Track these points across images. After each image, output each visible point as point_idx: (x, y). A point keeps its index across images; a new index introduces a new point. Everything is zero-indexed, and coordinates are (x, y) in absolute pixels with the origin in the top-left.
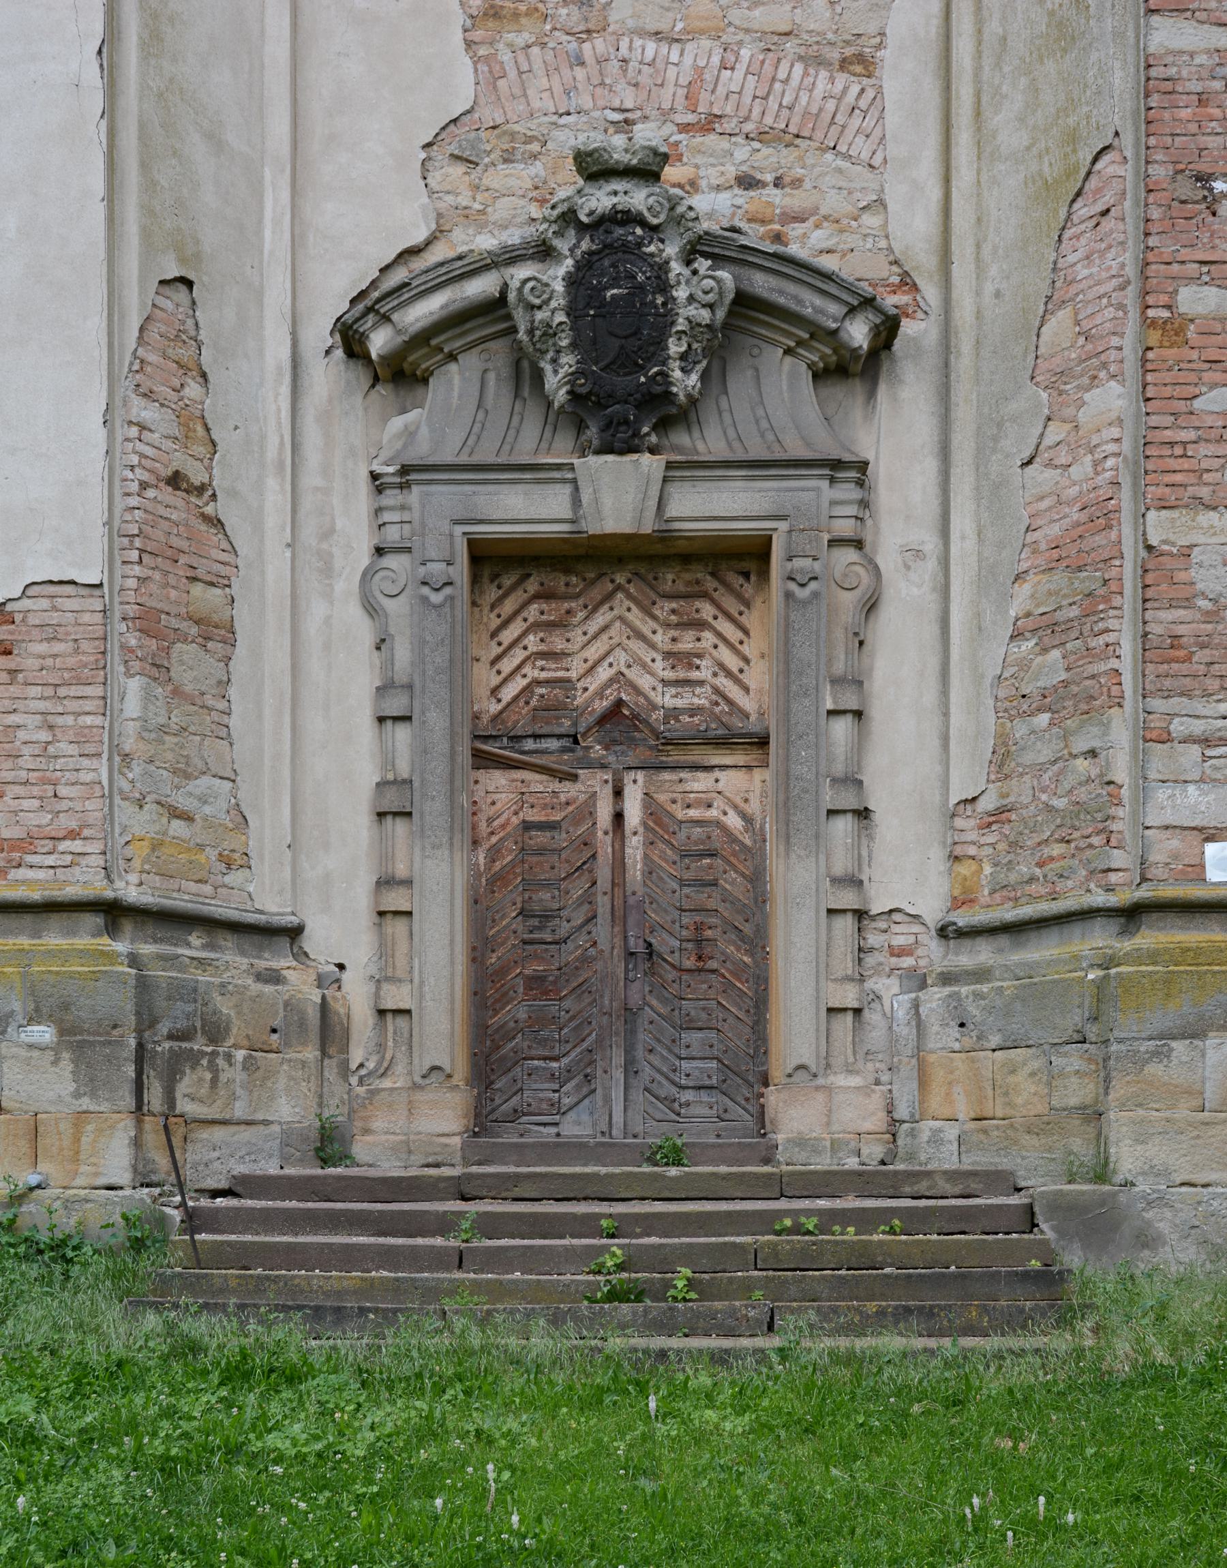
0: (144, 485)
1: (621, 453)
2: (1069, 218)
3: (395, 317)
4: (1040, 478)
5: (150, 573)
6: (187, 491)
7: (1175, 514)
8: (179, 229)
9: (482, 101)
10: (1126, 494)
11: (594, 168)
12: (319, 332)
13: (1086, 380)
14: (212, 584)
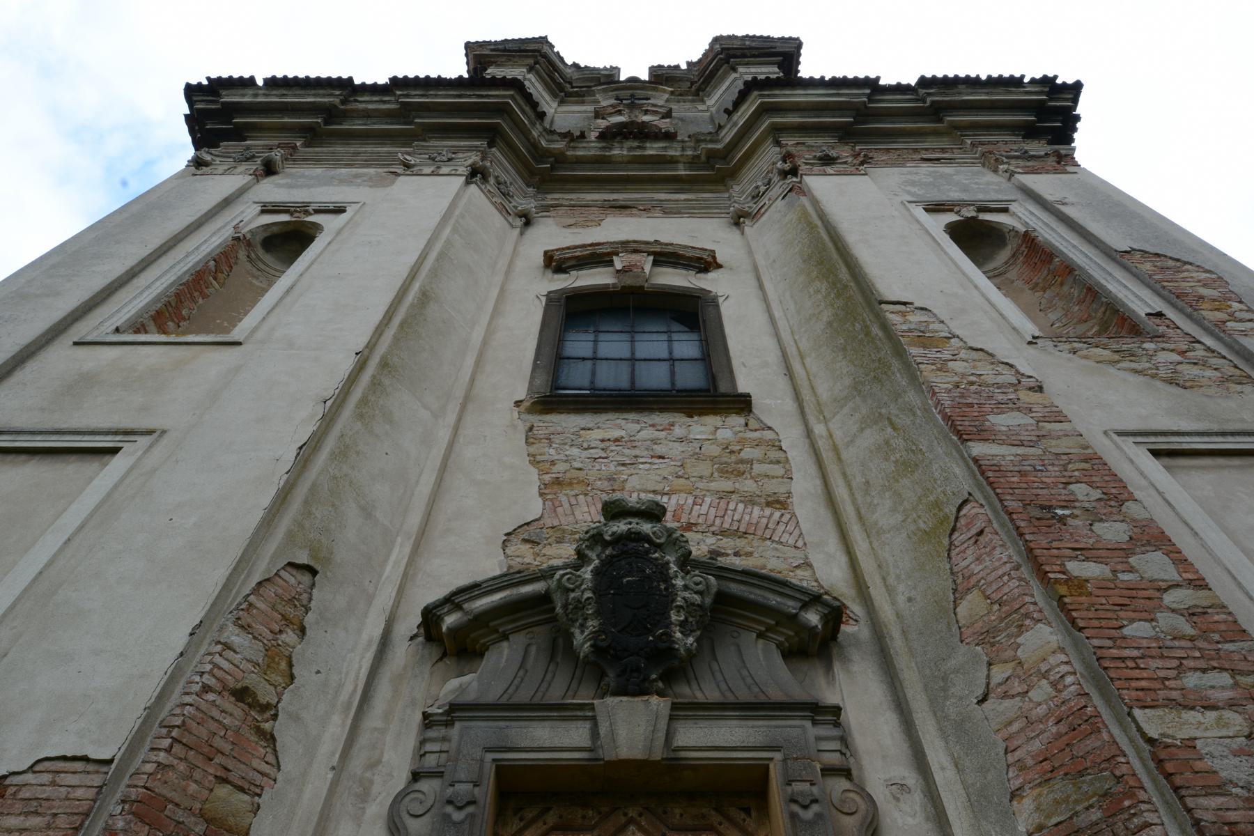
0: (206, 689)
1: (634, 695)
2: (951, 543)
3: (466, 606)
4: (1001, 708)
5: (175, 762)
6: (250, 705)
7: (1159, 712)
8: (319, 541)
9: (546, 516)
10: (1097, 700)
11: (614, 511)
12: (411, 621)
13: (1013, 630)
14: (242, 789)
